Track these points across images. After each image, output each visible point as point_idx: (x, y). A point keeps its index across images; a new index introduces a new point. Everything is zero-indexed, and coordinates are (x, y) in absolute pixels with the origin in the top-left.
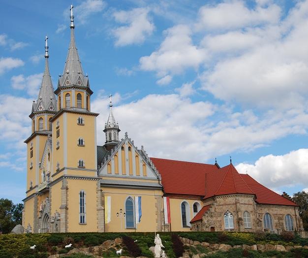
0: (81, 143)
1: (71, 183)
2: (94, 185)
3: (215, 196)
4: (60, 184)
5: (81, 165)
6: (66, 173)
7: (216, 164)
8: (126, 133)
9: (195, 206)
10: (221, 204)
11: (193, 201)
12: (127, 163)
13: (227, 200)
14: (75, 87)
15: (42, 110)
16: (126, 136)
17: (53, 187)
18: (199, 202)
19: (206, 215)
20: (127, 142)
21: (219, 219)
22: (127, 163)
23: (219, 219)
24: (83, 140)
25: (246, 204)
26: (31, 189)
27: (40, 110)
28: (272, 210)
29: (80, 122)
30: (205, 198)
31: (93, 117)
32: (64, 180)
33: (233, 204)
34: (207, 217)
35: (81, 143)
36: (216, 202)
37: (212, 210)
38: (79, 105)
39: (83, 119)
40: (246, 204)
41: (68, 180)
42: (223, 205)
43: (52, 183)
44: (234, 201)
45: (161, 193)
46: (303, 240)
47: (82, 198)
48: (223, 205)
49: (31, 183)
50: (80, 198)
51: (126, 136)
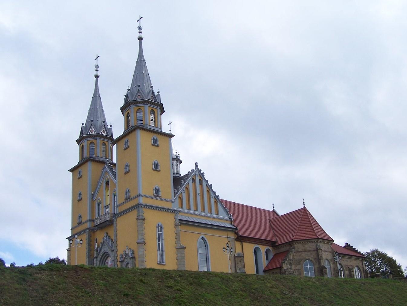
0: (156, 165)
1: (148, 214)
2: (168, 221)
3: (293, 241)
4: (133, 215)
5: (157, 194)
6: (142, 200)
7: (274, 210)
8: (196, 163)
9: (267, 252)
10: (299, 250)
11: (254, 245)
12: (199, 198)
13: (306, 246)
14: (148, 102)
15: (93, 133)
16: (196, 166)
17: (119, 219)
18: (270, 248)
19: (286, 262)
20: (197, 173)
21: (298, 267)
22: (199, 198)
23: (298, 267)
24: (159, 164)
25: (326, 251)
26: (80, 223)
27: (91, 133)
28: (344, 260)
29: (155, 141)
30: (278, 244)
31: (167, 138)
32: (140, 208)
33: (314, 251)
34: (287, 264)
35: (156, 165)
36: (294, 248)
37: (291, 257)
38: (155, 125)
39: (158, 139)
40: (326, 251)
41: (145, 210)
42: (302, 252)
43: (117, 214)
44: (314, 247)
45: (232, 236)
46: (109, 270)
47: (160, 232)
48: (302, 252)
49: (80, 217)
50: (163, 233)
51: (196, 166)
